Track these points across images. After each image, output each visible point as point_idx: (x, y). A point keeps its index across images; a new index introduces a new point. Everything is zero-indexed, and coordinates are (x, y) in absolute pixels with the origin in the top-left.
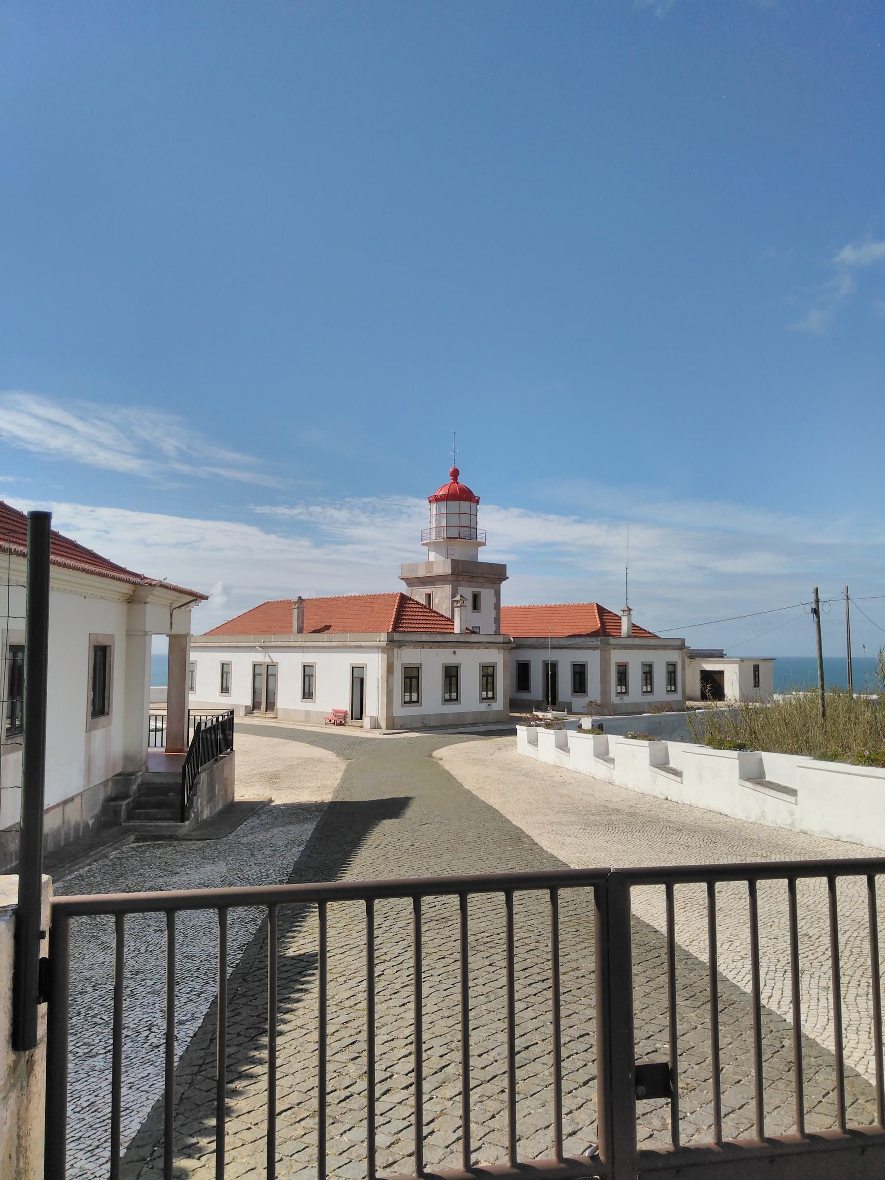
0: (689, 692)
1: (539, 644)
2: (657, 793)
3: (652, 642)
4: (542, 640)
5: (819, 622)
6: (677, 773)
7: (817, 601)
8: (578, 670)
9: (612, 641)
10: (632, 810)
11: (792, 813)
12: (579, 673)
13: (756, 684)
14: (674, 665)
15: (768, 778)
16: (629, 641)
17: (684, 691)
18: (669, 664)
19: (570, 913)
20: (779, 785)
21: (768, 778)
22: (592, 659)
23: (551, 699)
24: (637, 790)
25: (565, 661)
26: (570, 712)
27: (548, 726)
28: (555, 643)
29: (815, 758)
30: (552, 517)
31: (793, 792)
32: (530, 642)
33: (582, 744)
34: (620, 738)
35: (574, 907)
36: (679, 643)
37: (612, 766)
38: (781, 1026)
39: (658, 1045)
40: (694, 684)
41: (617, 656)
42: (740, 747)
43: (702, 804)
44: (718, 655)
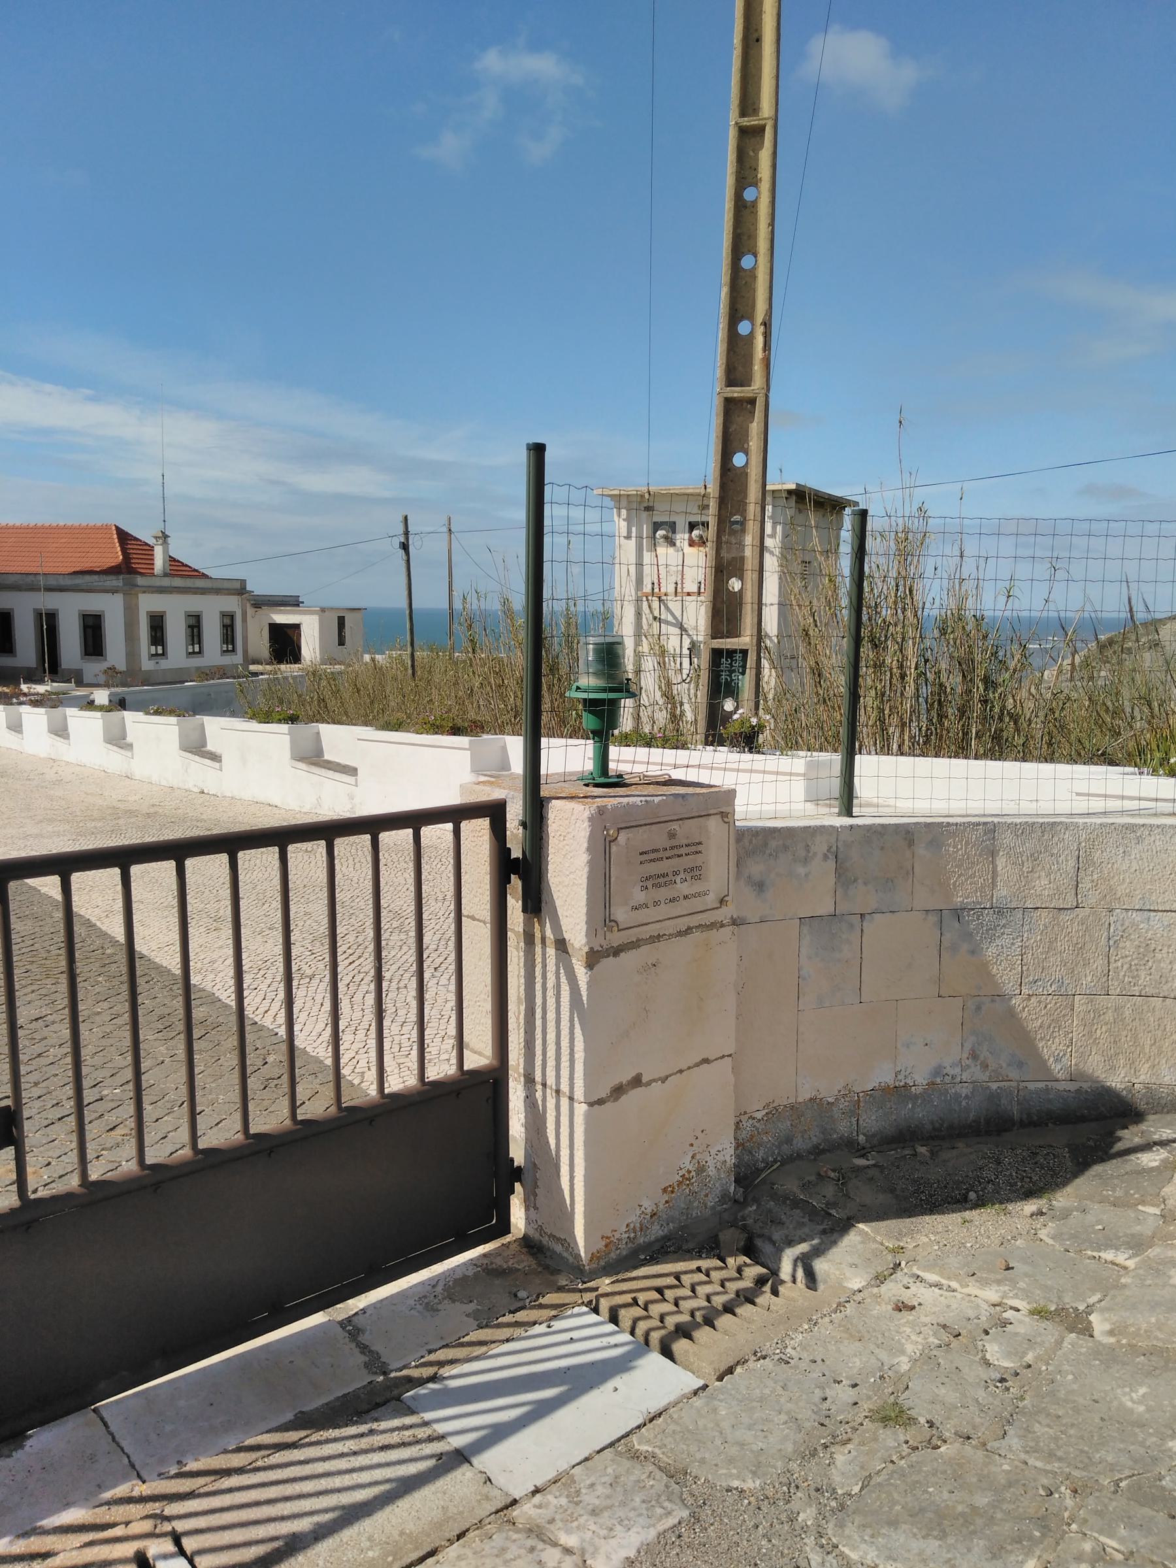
0: (252, 652)
1: (26, 584)
2: (190, 785)
3: (200, 583)
4: (31, 578)
5: (408, 561)
6: (215, 757)
7: (407, 533)
8: (90, 622)
9: (140, 581)
10: (152, 810)
11: (351, 797)
12: (93, 629)
13: (341, 642)
14: (232, 617)
15: (327, 757)
16: (166, 582)
17: (245, 652)
18: (224, 615)
19: (23, 950)
20: (339, 764)
21: (327, 757)
22: (111, 607)
23: (50, 664)
24: (164, 783)
25: (70, 612)
26: (80, 683)
27: (36, 703)
28: (52, 582)
29: (378, 729)
30: (48, 387)
31: (352, 771)
32: (11, 580)
33: (86, 726)
34: (140, 716)
35: (31, 942)
36: (238, 585)
37: (129, 754)
38: (274, 1040)
39: (105, 1092)
40: (260, 643)
41: (148, 603)
42: (293, 719)
43: (247, 795)
44: (292, 602)
